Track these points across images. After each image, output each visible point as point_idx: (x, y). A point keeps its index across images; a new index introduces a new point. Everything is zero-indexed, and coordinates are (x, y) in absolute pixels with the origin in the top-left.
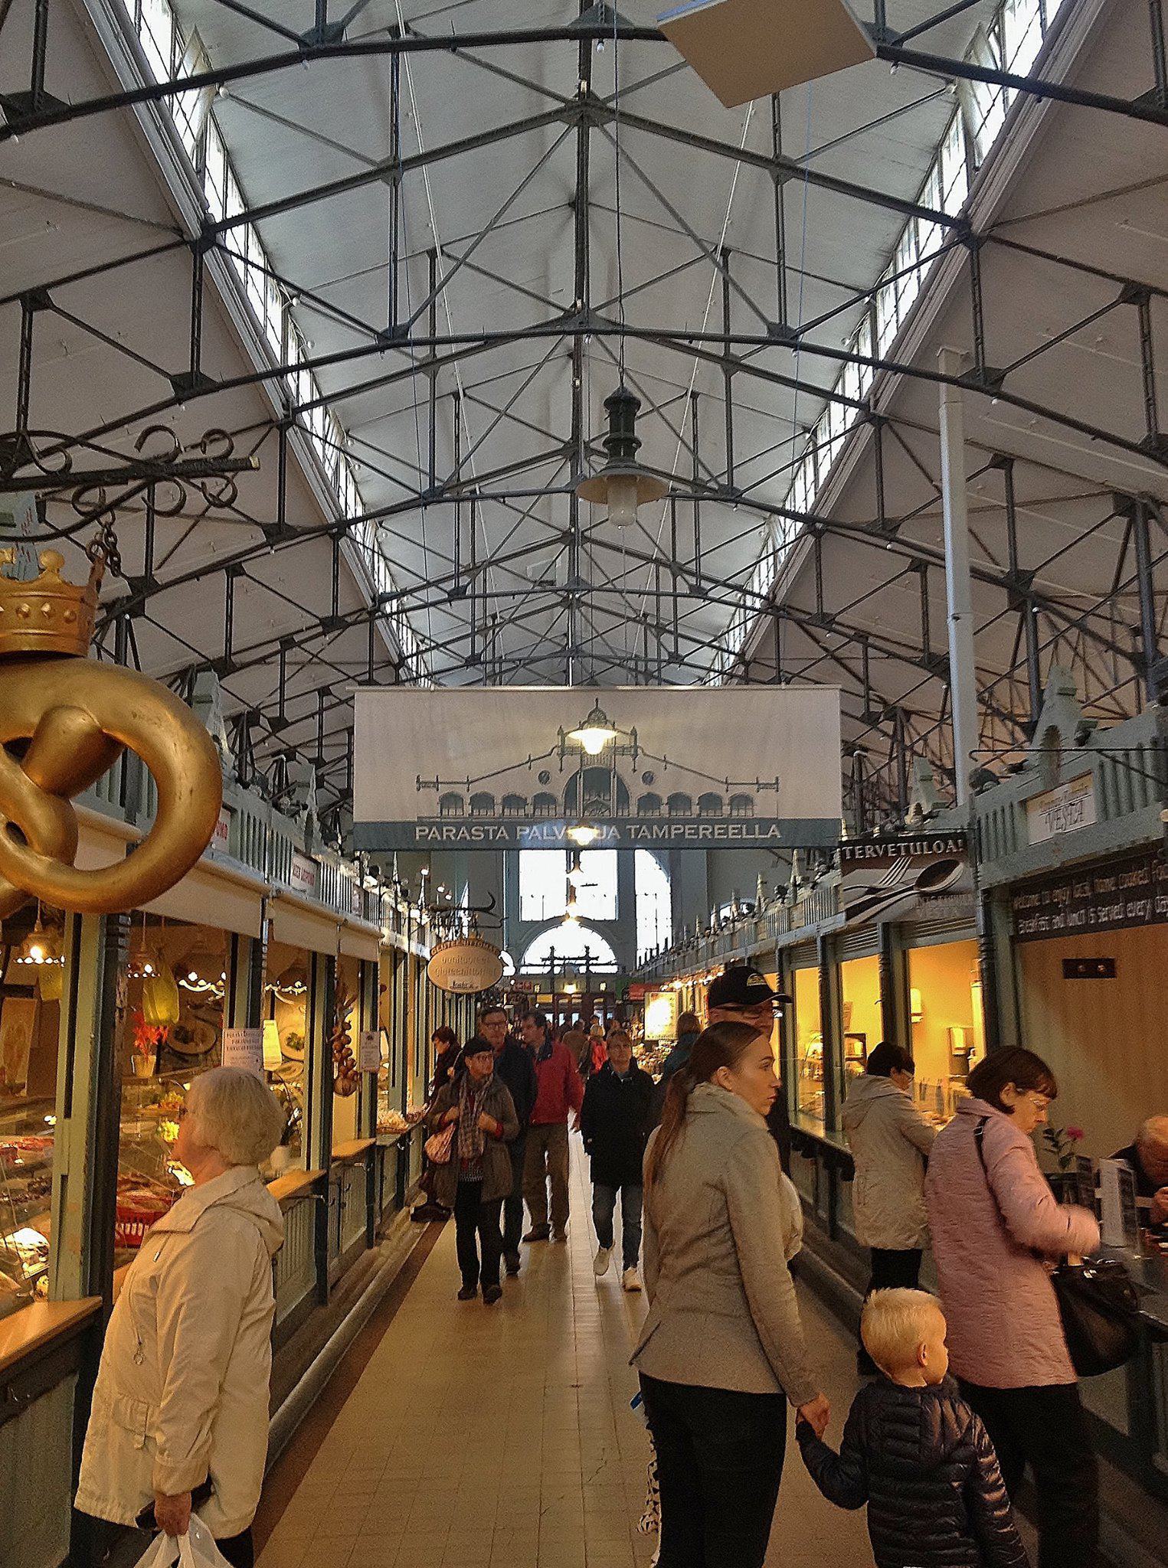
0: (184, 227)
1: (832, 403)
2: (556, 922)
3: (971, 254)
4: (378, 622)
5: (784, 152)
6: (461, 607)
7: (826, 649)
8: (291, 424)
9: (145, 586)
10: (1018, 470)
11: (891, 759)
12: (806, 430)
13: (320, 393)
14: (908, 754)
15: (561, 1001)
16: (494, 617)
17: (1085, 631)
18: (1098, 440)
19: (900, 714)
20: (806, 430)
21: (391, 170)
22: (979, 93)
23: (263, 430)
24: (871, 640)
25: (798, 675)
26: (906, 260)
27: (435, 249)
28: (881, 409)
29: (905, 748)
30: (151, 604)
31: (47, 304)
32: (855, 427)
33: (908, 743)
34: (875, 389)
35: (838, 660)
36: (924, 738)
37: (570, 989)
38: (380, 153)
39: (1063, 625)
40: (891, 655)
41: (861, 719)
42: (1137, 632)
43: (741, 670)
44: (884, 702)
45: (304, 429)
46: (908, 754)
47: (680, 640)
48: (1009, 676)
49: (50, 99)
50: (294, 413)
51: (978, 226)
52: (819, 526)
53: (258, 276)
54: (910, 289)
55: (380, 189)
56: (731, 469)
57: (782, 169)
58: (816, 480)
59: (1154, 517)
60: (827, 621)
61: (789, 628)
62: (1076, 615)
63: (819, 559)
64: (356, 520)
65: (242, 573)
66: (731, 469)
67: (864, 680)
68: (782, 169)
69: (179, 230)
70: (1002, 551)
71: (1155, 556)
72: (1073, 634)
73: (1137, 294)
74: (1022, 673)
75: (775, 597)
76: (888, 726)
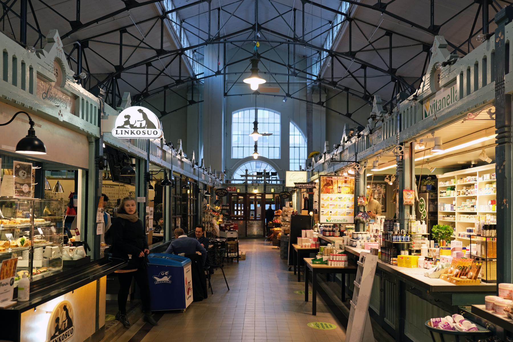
1: (338, 14)
2: (250, 159)
7: (349, 71)
8: (164, 18)
9: (120, 68)
12: (330, 22)
13: (175, 7)
15: (251, 197)
18: (353, 96)
20: (330, 22)
23: (156, 20)
27: (220, 8)
28: (352, 16)
30: (123, 75)
31: (126, 31)
32: (344, 21)
34: (350, 9)
37: (255, 191)
45: (169, 19)
50: (165, 13)
56: (304, 35)
58: (346, 9)
64: (187, 49)
65: (151, 65)
66: (304, 35)
75: (350, 15)
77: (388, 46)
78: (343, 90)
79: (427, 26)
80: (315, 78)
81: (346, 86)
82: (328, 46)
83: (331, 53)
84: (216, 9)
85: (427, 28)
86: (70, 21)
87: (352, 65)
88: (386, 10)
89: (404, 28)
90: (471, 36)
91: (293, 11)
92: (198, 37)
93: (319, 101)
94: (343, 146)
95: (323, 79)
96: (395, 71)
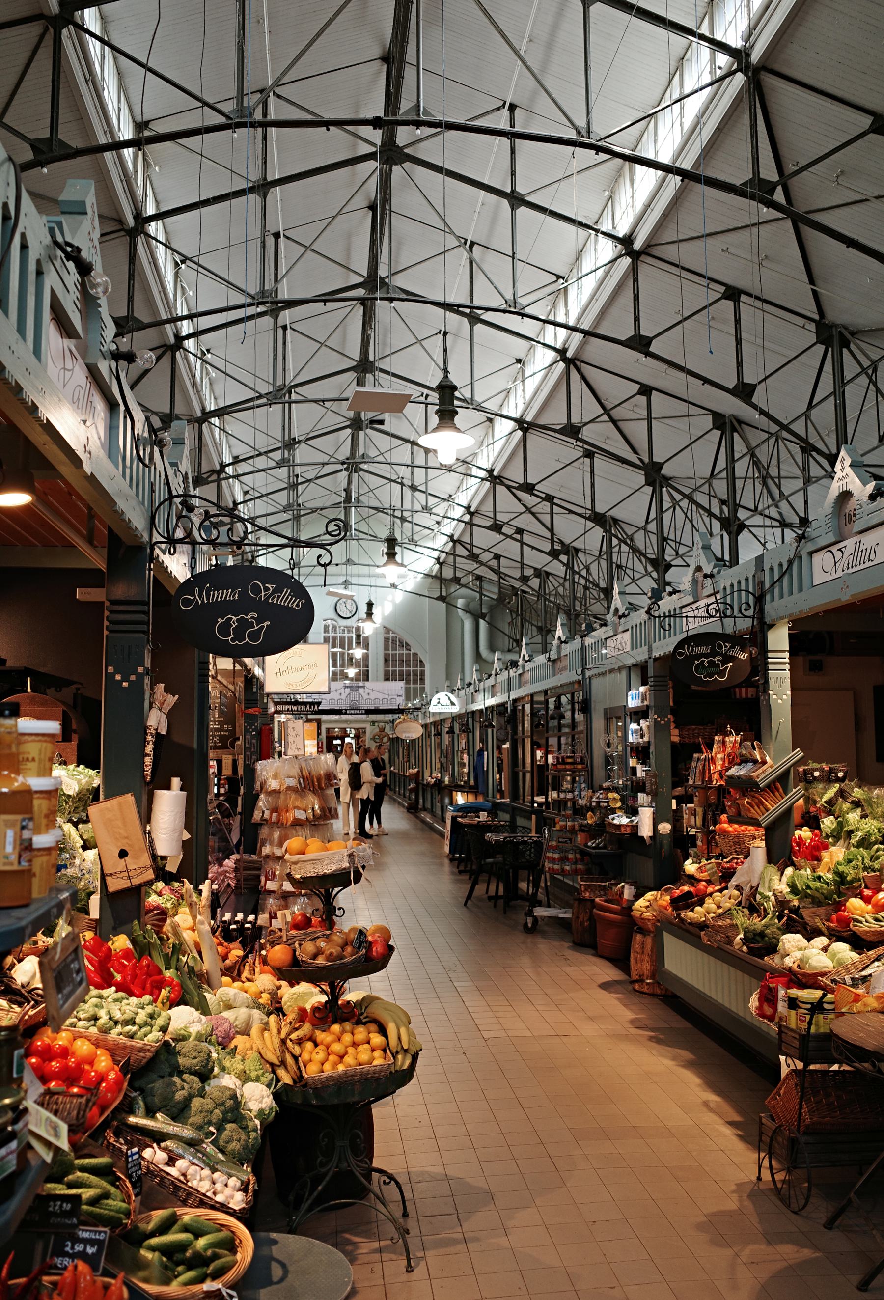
0: (123, 220)
3: (633, 261)
4: (224, 483)
5: (518, 189)
6: (283, 472)
7: (524, 506)
10: (598, 461)
11: (565, 579)
12: (519, 361)
14: (577, 577)
16: (297, 476)
17: (692, 501)
19: (543, 573)
20: (519, 361)
21: (263, 187)
22: (600, 246)
24: (555, 501)
25: (507, 523)
26: (587, 265)
29: (574, 572)
32: (613, 261)
33: (576, 568)
35: (533, 514)
36: (588, 568)
38: (255, 176)
39: (678, 497)
40: (571, 512)
41: (549, 554)
42: (723, 502)
43: (467, 518)
44: (562, 543)
46: (577, 577)
47: (430, 497)
48: (644, 528)
49: (63, 144)
50: (180, 338)
51: (638, 245)
52: (526, 426)
53: (199, 362)
54: (589, 284)
55: (253, 199)
57: (516, 200)
59: (737, 431)
60: (529, 488)
61: (501, 490)
62: (687, 491)
63: (525, 445)
67: (551, 530)
68: (516, 200)
69: (120, 221)
70: (643, 447)
71: (737, 456)
72: (685, 503)
73: (733, 294)
74: (652, 527)
76: (564, 558)
77: (505, 142)
78: (543, 499)
79: (731, 383)
80: (483, 474)
81: (645, 382)
82: (514, 408)
83: (520, 423)
84: (472, 330)
85: (731, 387)
86: (623, 339)
87: (570, 451)
88: (650, 349)
89: (674, 381)
90: (810, 406)
91: (441, 336)
92: (224, 373)
93: (438, 594)
94: (524, 667)
95: (499, 477)
96: (660, 466)
